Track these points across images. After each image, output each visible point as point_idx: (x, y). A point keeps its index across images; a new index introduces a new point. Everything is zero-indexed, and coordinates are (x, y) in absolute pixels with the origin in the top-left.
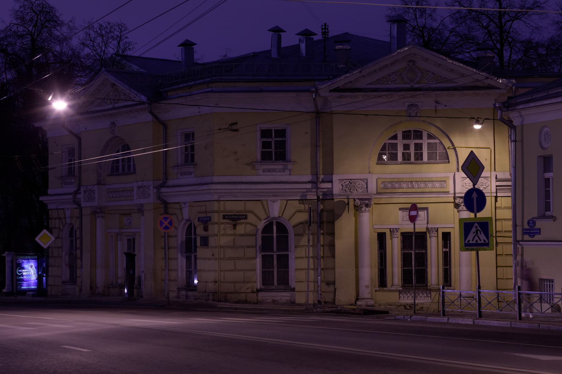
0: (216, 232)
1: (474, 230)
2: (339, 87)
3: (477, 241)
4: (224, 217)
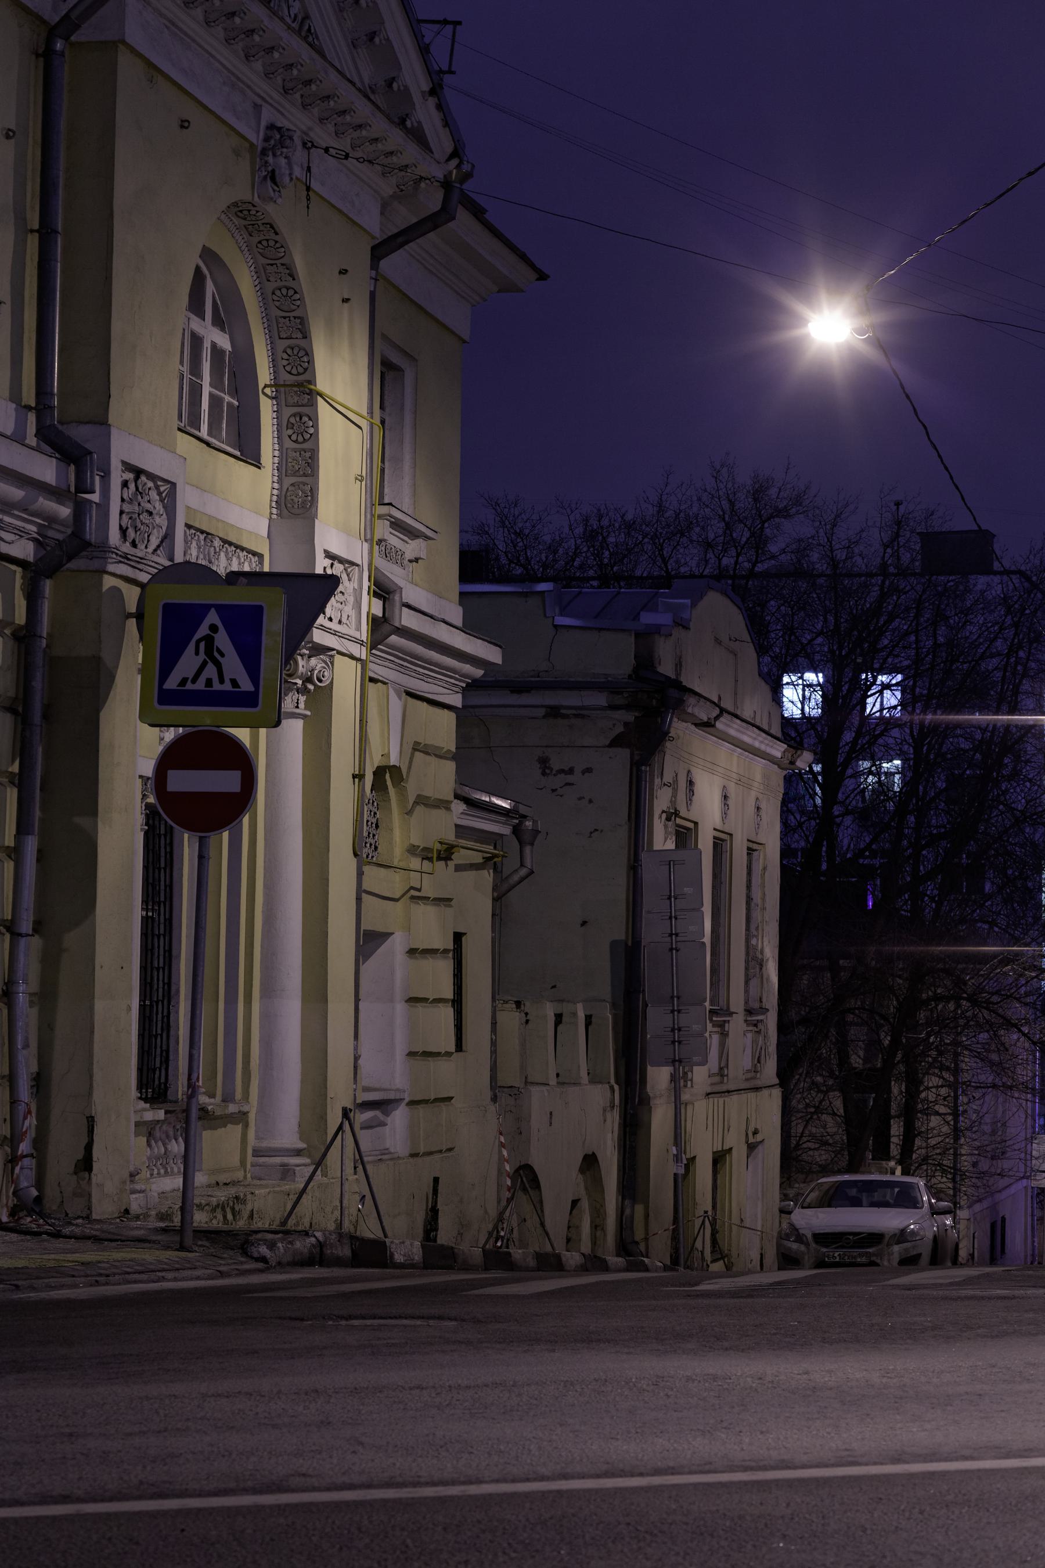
3: (209, 682)
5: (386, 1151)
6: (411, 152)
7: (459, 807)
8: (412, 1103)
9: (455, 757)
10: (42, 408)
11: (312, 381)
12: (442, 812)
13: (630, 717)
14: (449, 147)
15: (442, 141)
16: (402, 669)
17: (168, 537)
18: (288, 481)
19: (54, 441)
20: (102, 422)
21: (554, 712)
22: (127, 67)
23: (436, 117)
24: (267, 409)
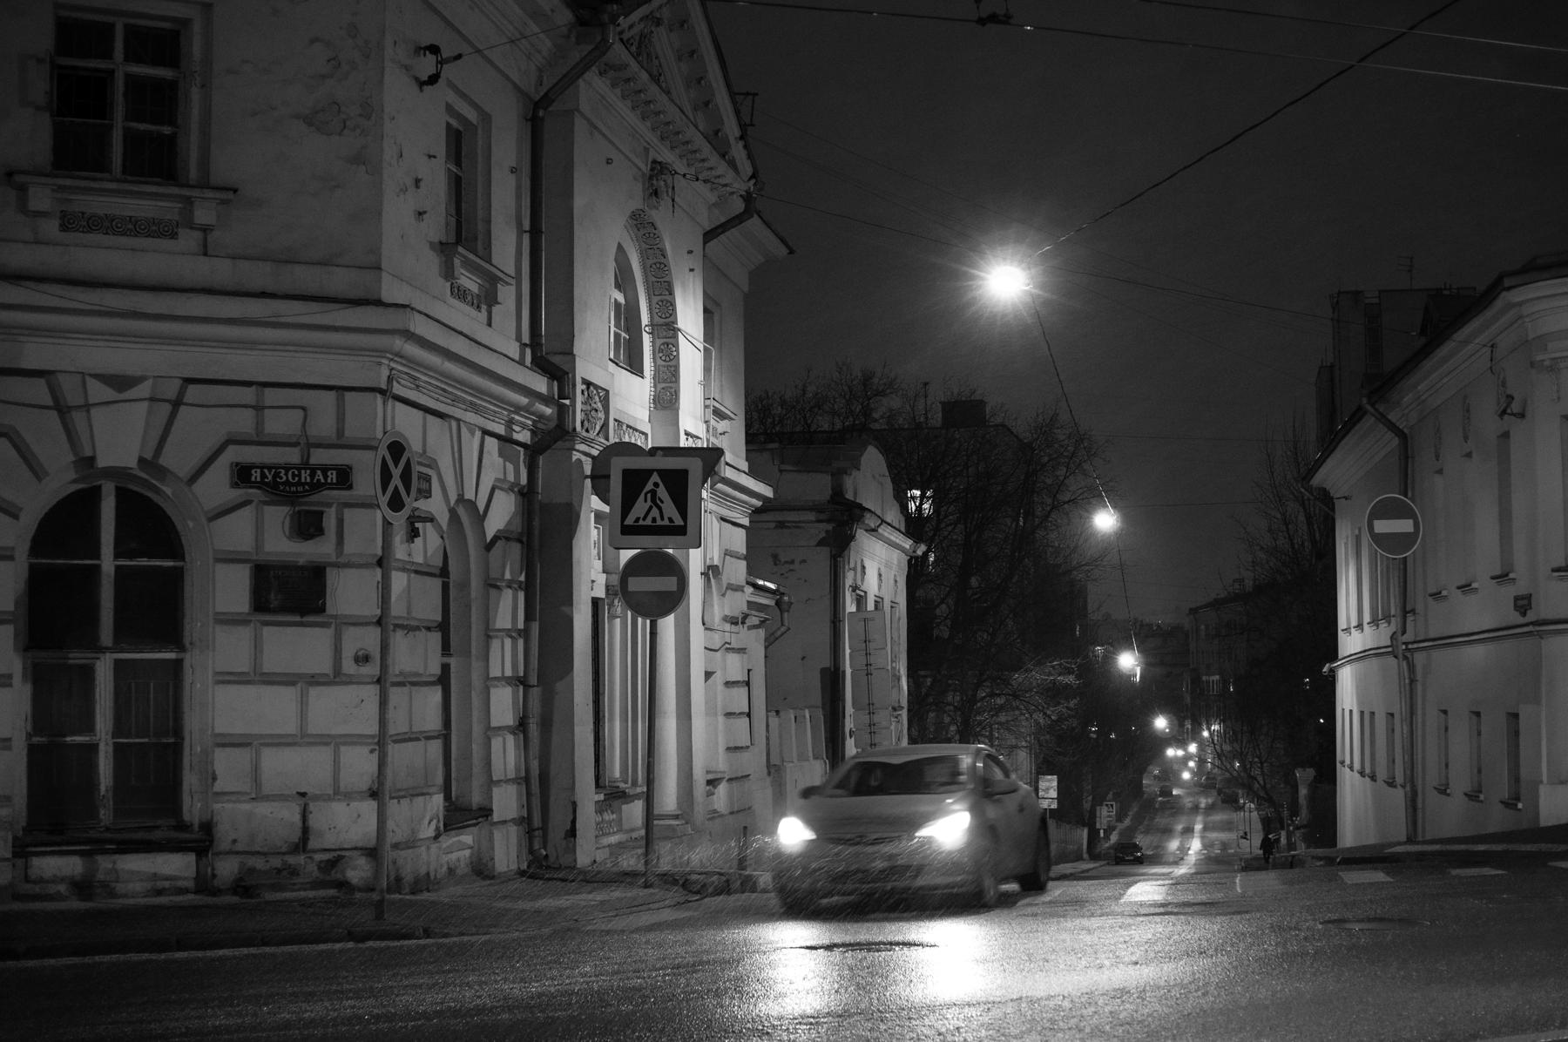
3: (654, 520)
5: (715, 811)
6: (730, 176)
7: (749, 590)
8: (730, 780)
9: (745, 558)
10: (535, 343)
11: (675, 322)
12: (739, 594)
13: (830, 527)
14: (750, 171)
15: (747, 169)
16: (719, 503)
17: (605, 426)
18: (660, 386)
19: (542, 364)
20: (570, 354)
21: (781, 525)
22: (580, 126)
23: (743, 153)
24: (647, 340)
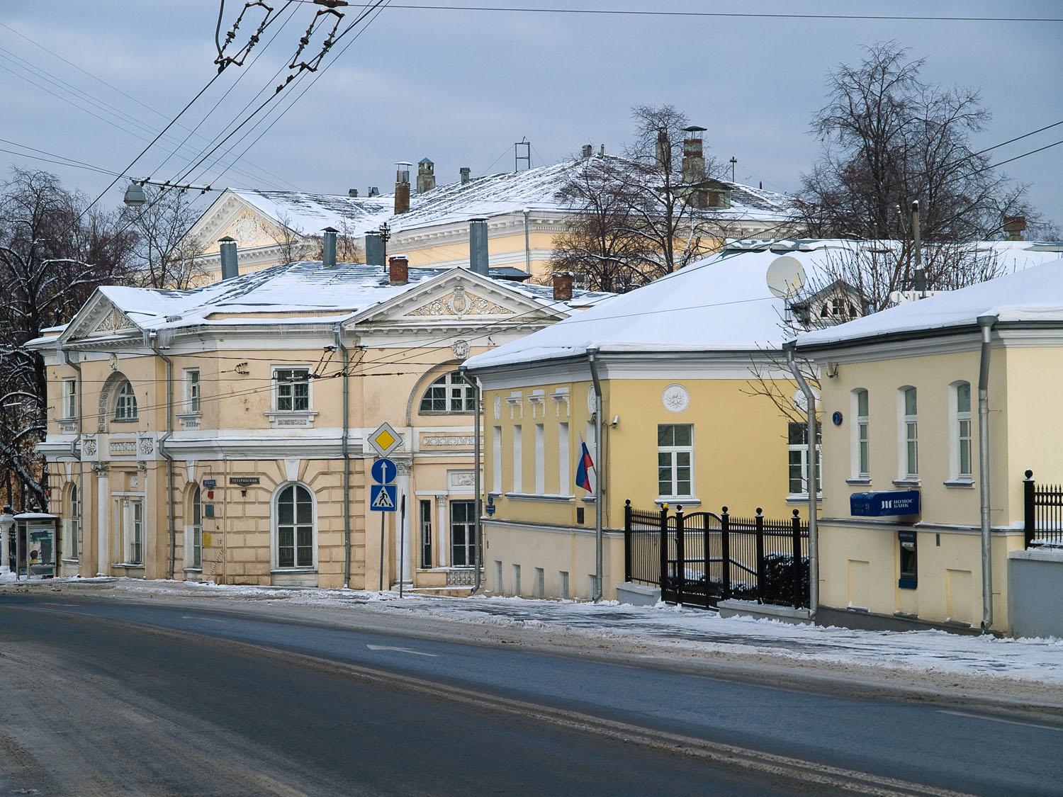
0: (221, 499)
1: (381, 494)
2: (368, 319)
3: (383, 504)
4: (232, 481)
